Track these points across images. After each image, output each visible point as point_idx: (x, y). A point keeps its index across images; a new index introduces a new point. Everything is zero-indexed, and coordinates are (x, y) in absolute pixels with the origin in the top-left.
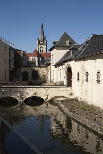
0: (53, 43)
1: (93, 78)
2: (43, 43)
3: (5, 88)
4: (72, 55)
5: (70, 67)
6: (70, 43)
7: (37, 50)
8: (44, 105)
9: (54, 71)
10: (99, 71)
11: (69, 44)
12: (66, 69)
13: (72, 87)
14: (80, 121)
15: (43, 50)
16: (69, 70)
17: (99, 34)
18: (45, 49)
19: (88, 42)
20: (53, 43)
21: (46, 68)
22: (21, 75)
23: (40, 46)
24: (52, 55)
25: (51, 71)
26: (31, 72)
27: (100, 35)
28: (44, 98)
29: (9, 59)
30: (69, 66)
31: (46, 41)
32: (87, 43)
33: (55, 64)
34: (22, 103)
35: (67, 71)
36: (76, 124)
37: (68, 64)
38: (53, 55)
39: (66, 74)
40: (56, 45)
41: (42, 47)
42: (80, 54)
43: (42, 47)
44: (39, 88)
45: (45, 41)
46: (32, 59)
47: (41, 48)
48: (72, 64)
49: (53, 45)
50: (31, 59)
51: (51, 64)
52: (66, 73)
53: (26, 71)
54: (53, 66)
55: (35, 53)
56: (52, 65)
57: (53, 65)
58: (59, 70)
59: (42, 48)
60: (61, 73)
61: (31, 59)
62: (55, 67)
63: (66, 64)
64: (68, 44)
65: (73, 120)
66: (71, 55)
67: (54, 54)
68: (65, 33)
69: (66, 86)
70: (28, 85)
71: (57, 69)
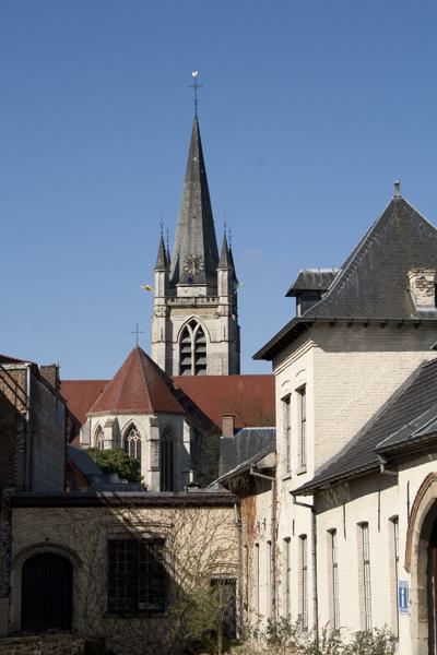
0: (289, 294)
2: (203, 291)
7: (157, 354)
9: (303, 537)
12: (411, 519)
15: (204, 355)
20: (289, 294)
21: (230, 514)
23: (179, 320)
24: (287, 399)
25: (280, 543)
26: (102, 546)
31: (233, 279)
33: (309, 477)
35: (422, 536)
38: (295, 397)
40: (320, 310)
43: (193, 324)
45: (222, 276)
46: (108, 433)
49: (290, 311)
51: (280, 473)
52: (414, 558)
53: (55, 538)
54: (295, 493)
55: (139, 382)
56: (283, 489)
57: (298, 482)
58: (353, 530)
59: (193, 334)
62: (309, 500)
67: (302, 390)
71: (330, 518)
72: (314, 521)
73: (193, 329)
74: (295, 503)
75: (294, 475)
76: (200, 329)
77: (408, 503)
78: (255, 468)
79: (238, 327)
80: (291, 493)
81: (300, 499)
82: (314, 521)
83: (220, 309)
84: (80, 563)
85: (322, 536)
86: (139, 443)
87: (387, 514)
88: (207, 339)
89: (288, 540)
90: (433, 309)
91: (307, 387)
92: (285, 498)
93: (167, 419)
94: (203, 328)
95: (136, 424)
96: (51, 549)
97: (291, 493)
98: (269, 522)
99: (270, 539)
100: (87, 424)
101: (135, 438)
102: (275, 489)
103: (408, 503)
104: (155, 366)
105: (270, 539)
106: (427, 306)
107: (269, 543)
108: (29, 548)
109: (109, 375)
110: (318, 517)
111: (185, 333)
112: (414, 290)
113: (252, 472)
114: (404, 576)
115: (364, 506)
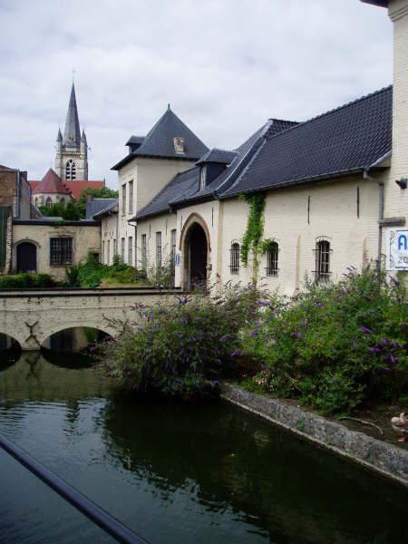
0: (127, 145)
1: (298, 260)
2: (75, 150)
4: (207, 184)
5: (201, 224)
7: (57, 172)
9: (131, 238)
10: (325, 239)
12: (182, 232)
14: (284, 425)
16: (196, 240)
18: (82, 171)
19: (260, 141)
20: (127, 145)
21: (96, 229)
22: (208, 382)
23: (66, 160)
25: (120, 240)
26: (48, 240)
27: (296, 123)
29: (391, 83)
30: (194, 219)
31: (86, 145)
32: (256, 147)
33: (134, 215)
34: (36, 355)
35: (187, 236)
37: (193, 215)
38: (128, 185)
41: (71, 161)
42: (237, 182)
44: (96, 298)
45: (82, 144)
46: (40, 200)
47: (68, 165)
48: (209, 215)
49: (126, 152)
50: (36, 199)
51: (121, 213)
53: (29, 238)
55: (52, 181)
57: (131, 217)
58: (154, 236)
59: (71, 164)
61: (36, 199)
62: (134, 223)
66: (203, 184)
67: (131, 182)
68: (26, 172)
69: (182, 291)
70: (47, 287)
71: (144, 229)
72: (381, 232)
82: (381, 232)
84: (40, 247)
88: (76, 167)
93: (61, 196)
102: (67, 225)
104: (56, 175)
109: (40, 180)
111: (68, 165)
112: (176, 145)
115: (158, 224)
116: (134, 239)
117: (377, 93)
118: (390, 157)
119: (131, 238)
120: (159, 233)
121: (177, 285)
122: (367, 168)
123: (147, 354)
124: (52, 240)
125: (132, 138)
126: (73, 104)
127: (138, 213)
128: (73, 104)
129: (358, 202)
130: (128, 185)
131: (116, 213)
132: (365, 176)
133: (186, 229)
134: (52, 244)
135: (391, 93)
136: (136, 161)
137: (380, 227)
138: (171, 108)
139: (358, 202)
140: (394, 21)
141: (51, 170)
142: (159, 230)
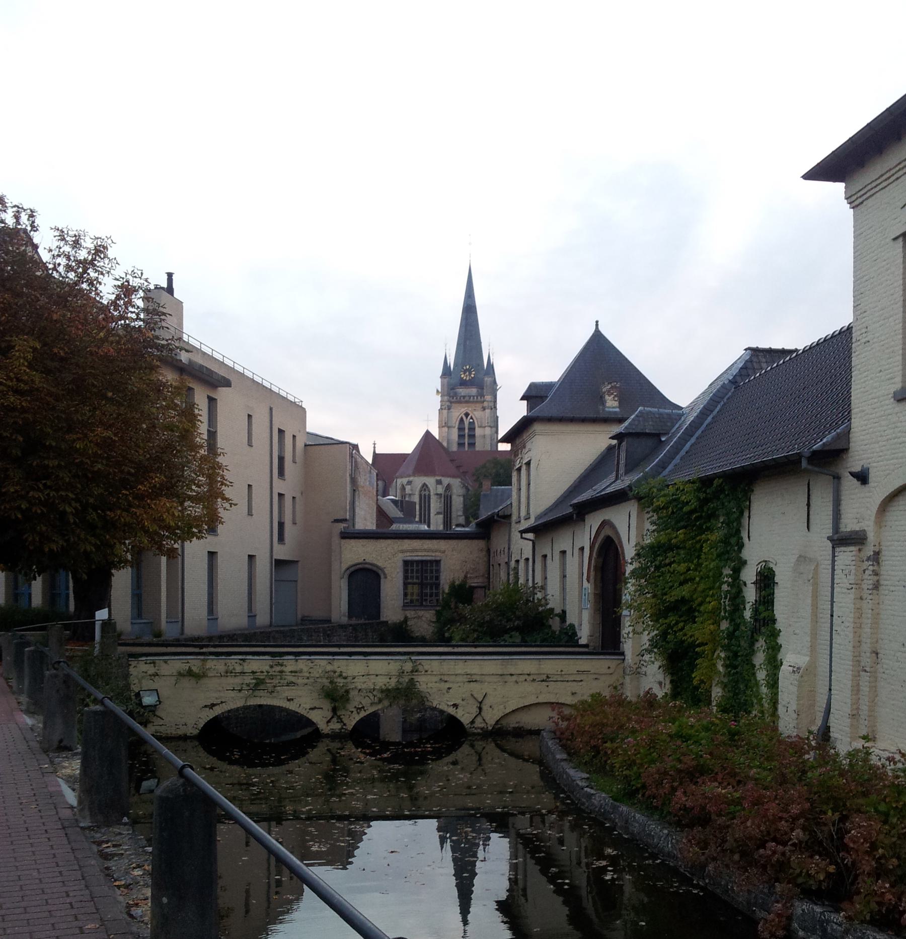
0: (523, 399)
3: (898, 446)
6: (623, 400)
7: (436, 433)
8: (464, 753)
11: (616, 404)
13: (623, 654)
15: (474, 436)
17: (787, 348)
20: (523, 399)
23: (458, 412)
24: (519, 470)
25: (513, 564)
26: (400, 564)
27: (790, 352)
28: (464, 716)
30: (607, 532)
33: (531, 522)
36: (288, 871)
37: (605, 524)
38: (524, 468)
39: (592, 578)
40: (542, 409)
41: (467, 415)
43: (467, 415)
51: (514, 518)
52: (592, 573)
54: (522, 532)
56: (516, 529)
57: (525, 525)
58: (557, 556)
59: (466, 422)
60: (565, 576)
62: (530, 536)
63: (594, 521)
64: (611, 404)
65: (274, 855)
72: (834, 556)
73: (467, 418)
74: (522, 538)
75: (522, 521)
76: (472, 418)
77: (590, 539)
78: (498, 515)
79: (497, 417)
80: (519, 531)
81: (524, 535)
82: (834, 556)
83: (485, 404)
84: (385, 574)
85: (538, 559)
86: (429, 496)
87: (578, 545)
89: (517, 561)
90: (617, 410)
91: (532, 462)
92: (516, 535)
94: (473, 417)
95: (427, 483)
96: (367, 566)
97: (519, 531)
98: (506, 550)
99: (507, 560)
100: (394, 483)
101: (427, 493)
103: (590, 539)
105: (507, 560)
106: (614, 408)
107: (506, 563)
108: (348, 569)
110: (837, 549)
113: (495, 518)
114: (586, 584)
116: (531, 560)
117: (841, 332)
118: (848, 431)
119: (527, 559)
120: (545, 556)
121: (583, 641)
122: (806, 452)
123: (735, 778)
124: (406, 563)
125: (533, 387)
126: (469, 311)
127: (537, 518)
128: (469, 311)
129: (808, 505)
130: (524, 468)
131: (509, 517)
132: (804, 464)
133: (597, 546)
134: (406, 571)
135: (851, 333)
136: (537, 427)
137: (833, 548)
138: (600, 328)
139: (808, 505)
140: (853, 208)
141: (428, 434)
142: (544, 553)
